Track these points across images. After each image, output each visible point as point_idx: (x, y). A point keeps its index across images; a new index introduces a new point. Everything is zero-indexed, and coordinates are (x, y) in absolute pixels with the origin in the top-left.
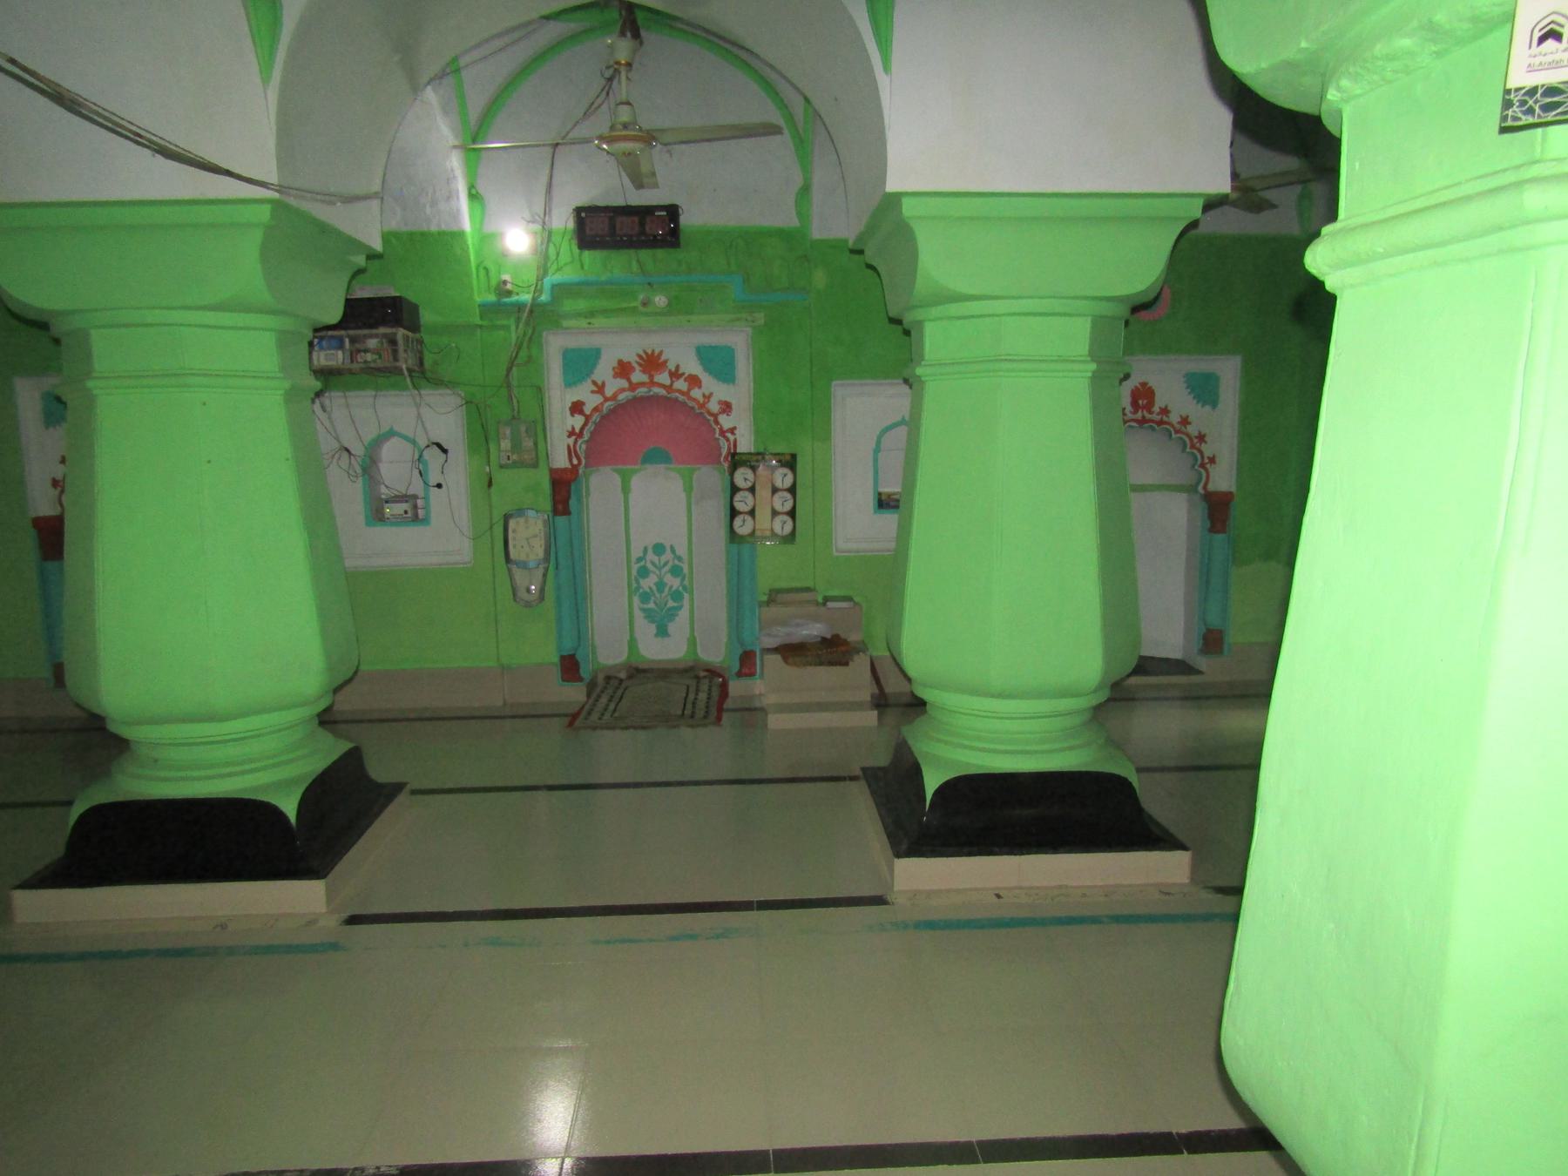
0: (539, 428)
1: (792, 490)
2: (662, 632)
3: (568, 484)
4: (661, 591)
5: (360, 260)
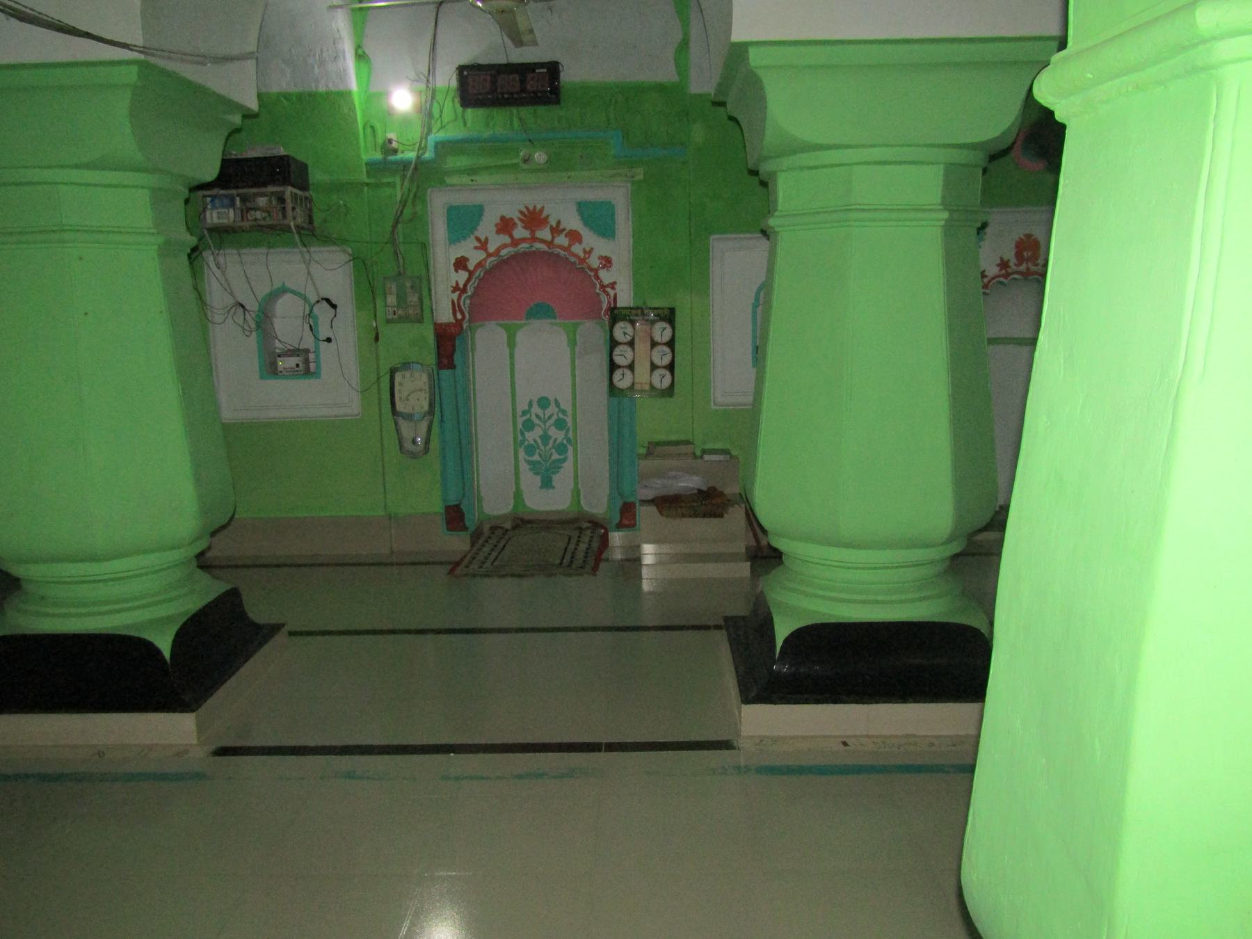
0: (425, 283)
1: (671, 344)
2: (547, 484)
3: (452, 338)
4: (545, 444)
5: (237, 119)
